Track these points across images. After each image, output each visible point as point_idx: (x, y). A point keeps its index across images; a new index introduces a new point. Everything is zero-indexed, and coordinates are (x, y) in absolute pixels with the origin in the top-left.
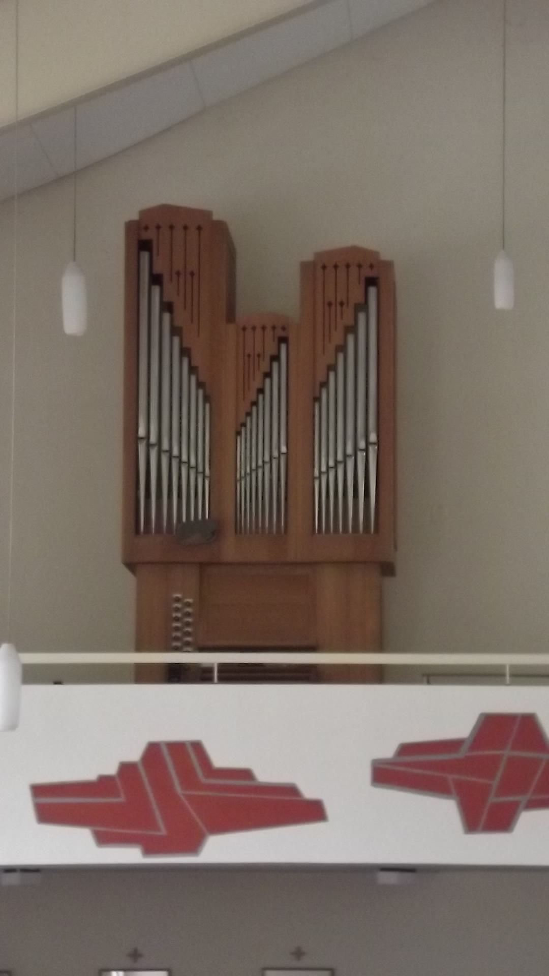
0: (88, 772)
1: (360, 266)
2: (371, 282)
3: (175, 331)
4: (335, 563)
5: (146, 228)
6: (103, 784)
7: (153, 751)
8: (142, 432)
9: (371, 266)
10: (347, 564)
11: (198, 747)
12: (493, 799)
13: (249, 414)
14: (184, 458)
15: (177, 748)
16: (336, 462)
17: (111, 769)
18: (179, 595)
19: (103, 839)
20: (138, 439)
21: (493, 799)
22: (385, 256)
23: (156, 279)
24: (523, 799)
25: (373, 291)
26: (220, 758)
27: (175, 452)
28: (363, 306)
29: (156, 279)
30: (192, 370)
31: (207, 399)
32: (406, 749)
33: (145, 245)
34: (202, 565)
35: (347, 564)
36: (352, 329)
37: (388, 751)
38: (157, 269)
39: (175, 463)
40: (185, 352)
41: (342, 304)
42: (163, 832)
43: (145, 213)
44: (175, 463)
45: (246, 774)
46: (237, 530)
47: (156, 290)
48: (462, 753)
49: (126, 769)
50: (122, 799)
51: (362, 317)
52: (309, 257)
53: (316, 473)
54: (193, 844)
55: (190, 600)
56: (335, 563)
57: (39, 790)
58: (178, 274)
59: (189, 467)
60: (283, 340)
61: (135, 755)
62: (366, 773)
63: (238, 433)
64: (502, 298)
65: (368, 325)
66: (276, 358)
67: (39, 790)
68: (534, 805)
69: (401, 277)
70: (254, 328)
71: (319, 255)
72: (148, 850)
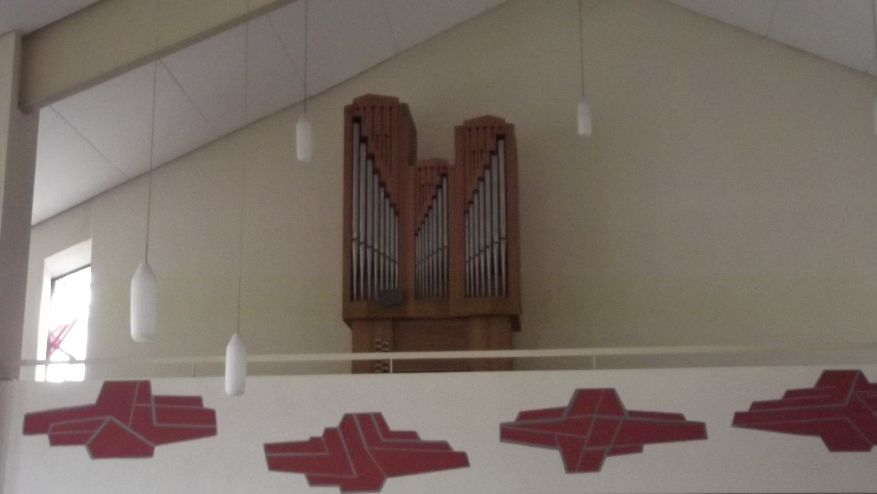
0: (302, 434)
1: (492, 127)
2: (500, 137)
3: (375, 171)
4: (477, 316)
5: (358, 109)
7: (348, 420)
8: (355, 235)
9: (500, 128)
10: (487, 317)
11: (379, 417)
12: (586, 449)
13: (423, 222)
14: (382, 251)
15: (365, 418)
16: (480, 251)
17: (319, 433)
18: (380, 340)
20: (352, 240)
21: (586, 449)
22: (509, 120)
23: (363, 140)
24: (607, 448)
25: (501, 143)
26: (394, 425)
27: (376, 247)
28: (494, 153)
29: (363, 140)
30: (387, 195)
31: (397, 213)
32: (524, 416)
33: (357, 120)
34: (395, 320)
35: (487, 317)
36: (488, 167)
37: (511, 417)
38: (365, 133)
39: (376, 255)
40: (382, 184)
41: (481, 151)
42: (355, 475)
43: (356, 101)
44: (376, 255)
45: (413, 435)
46: (417, 296)
47: (370, 163)
48: (564, 417)
49: (330, 433)
50: (326, 453)
51: (494, 159)
52: (460, 123)
53: (467, 259)
55: (387, 343)
56: (477, 316)
57: (270, 448)
58: (378, 136)
60: (444, 175)
61: (335, 422)
62: (497, 433)
63: (416, 235)
64: (584, 127)
65: (499, 164)
66: (440, 186)
67: (270, 448)
68: (615, 452)
69: (521, 134)
70: (426, 169)
71: (466, 122)
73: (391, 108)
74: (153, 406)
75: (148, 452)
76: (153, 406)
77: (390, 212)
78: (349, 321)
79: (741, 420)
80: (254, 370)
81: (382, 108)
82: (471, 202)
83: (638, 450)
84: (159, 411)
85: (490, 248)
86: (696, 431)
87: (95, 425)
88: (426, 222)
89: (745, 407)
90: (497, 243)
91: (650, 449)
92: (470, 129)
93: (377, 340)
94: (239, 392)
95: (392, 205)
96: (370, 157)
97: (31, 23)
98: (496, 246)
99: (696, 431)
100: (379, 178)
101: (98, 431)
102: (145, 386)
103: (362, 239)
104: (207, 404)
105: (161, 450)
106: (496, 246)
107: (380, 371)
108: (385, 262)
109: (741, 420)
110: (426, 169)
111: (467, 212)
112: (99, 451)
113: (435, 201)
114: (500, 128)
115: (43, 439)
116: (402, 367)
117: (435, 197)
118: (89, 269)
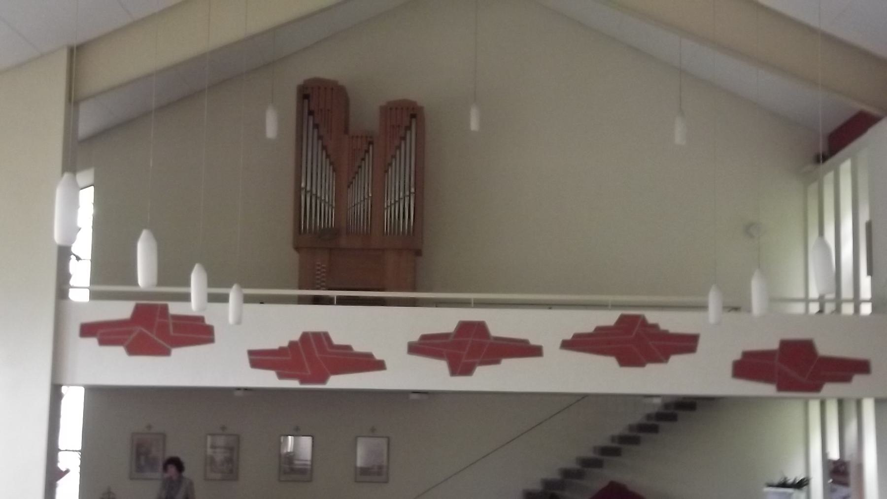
2: (413, 116)
6: (281, 351)
7: (305, 337)
8: (303, 185)
9: (413, 109)
11: (326, 335)
17: (285, 344)
19: (281, 376)
23: (311, 113)
25: (414, 121)
28: (409, 128)
29: (311, 113)
30: (328, 156)
31: (334, 170)
37: (415, 338)
40: (324, 148)
42: (309, 373)
45: (348, 348)
48: (451, 339)
49: (292, 344)
51: (408, 132)
54: (323, 380)
57: (251, 353)
59: (316, 197)
60: (371, 143)
61: (296, 337)
62: (405, 348)
63: (349, 187)
65: (412, 136)
66: (367, 151)
67: (251, 353)
72: (303, 381)
73: (332, 89)
74: (171, 322)
75: (166, 353)
76: (171, 322)
77: (330, 169)
78: (297, 248)
79: (567, 345)
80: (248, 299)
81: (326, 88)
82: (390, 164)
83: (497, 362)
84: (175, 325)
85: (403, 200)
86: (535, 351)
87: (130, 333)
88: (357, 178)
89: (569, 337)
90: (408, 196)
91: (506, 362)
92: (396, 109)
93: (318, 263)
94: (239, 322)
95: (331, 164)
96: (316, 126)
97: (75, 41)
98: (407, 199)
99: (535, 351)
100: (318, 132)
101: (132, 337)
102: (165, 308)
103: (308, 188)
104: (208, 321)
105: (176, 352)
106: (407, 199)
107: (324, 289)
108: (325, 197)
109: (567, 345)
110: (357, 137)
111: (387, 171)
112: (133, 350)
113: (363, 162)
114: (413, 109)
115: (93, 342)
116: (343, 301)
117: (363, 159)
118: (92, 188)
